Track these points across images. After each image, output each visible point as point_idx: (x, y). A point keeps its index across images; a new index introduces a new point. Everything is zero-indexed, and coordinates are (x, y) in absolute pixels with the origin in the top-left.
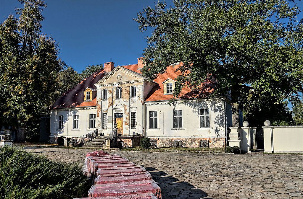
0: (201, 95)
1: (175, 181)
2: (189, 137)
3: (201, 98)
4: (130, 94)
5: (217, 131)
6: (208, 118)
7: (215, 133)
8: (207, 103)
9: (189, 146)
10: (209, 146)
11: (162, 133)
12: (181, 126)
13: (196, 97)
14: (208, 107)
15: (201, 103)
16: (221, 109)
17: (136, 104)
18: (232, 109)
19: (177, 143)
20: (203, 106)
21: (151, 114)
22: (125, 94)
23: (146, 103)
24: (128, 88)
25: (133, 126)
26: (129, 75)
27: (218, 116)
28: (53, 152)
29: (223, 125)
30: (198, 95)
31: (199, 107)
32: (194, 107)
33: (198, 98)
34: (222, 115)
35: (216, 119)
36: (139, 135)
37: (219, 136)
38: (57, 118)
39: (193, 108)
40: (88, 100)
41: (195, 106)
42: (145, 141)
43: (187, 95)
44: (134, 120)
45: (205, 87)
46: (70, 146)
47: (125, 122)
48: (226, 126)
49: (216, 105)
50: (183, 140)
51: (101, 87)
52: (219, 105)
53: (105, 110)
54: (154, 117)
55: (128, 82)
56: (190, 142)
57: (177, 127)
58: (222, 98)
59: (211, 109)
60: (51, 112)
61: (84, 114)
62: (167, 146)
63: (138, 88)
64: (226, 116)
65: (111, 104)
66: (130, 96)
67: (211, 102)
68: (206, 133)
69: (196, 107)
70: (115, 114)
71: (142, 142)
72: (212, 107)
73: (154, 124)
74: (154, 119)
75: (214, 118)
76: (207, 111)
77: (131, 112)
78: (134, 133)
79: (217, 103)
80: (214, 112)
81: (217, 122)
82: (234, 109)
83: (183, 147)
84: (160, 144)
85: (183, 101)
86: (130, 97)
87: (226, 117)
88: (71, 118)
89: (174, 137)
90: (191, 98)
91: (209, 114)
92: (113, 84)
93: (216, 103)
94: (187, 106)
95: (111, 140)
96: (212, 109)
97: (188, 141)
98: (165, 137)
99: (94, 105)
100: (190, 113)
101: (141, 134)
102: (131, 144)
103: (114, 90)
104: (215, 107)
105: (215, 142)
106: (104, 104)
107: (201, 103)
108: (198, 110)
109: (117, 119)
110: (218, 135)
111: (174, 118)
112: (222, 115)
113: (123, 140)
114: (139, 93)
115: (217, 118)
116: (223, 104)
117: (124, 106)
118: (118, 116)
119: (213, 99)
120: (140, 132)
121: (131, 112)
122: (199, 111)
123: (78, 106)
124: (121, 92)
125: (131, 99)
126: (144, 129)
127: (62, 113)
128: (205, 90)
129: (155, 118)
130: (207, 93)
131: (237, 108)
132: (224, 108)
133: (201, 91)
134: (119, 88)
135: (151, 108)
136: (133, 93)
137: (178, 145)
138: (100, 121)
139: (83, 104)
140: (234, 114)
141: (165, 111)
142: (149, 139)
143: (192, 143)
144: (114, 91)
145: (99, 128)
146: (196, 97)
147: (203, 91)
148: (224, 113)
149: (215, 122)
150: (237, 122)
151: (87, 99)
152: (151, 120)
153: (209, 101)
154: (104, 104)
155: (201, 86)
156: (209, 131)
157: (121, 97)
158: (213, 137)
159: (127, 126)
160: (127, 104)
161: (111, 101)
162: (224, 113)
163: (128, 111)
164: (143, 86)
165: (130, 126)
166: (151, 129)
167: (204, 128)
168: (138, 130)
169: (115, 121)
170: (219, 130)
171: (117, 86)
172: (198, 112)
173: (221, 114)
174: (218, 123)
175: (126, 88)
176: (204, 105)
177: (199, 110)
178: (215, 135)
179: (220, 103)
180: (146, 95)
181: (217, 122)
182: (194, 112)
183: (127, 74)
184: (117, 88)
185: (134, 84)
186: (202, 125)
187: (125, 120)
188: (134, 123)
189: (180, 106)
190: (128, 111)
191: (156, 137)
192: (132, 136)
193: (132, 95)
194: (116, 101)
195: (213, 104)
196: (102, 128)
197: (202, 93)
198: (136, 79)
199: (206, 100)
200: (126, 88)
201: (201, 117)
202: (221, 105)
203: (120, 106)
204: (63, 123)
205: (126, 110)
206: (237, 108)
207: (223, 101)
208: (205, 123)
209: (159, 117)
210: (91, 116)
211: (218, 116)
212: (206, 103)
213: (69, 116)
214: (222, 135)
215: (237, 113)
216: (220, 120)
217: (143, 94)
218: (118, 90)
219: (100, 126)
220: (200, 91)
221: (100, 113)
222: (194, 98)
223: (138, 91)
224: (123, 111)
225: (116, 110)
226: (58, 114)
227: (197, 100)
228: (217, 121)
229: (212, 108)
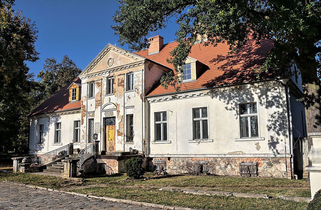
0: (239, 78)
2: (220, 156)
3: (240, 83)
4: (125, 85)
5: (273, 144)
6: (255, 120)
7: (270, 147)
8: (253, 92)
9: (220, 173)
10: (257, 174)
11: (176, 148)
12: (206, 136)
13: (231, 81)
14: (253, 98)
15: (241, 93)
16: (280, 100)
18: (305, 97)
19: (200, 167)
20: (245, 98)
21: (157, 115)
22: (119, 86)
23: (148, 99)
24: (122, 77)
25: (130, 138)
27: (274, 115)
29: (285, 132)
30: (235, 79)
31: (237, 100)
32: (229, 101)
33: (235, 84)
34: (283, 112)
35: (269, 121)
36: (137, 152)
37: (279, 154)
38: (37, 128)
39: (226, 102)
40: (74, 100)
41: (230, 99)
42: (131, 165)
43: (216, 80)
44: (132, 128)
45: (246, 67)
46: (21, 171)
48: (291, 133)
49: (269, 93)
50: (210, 160)
52: (275, 94)
54: (162, 122)
55: (122, 68)
56: (223, 165)
57: (199, 137)
58: (281, 80)
59: (261, 103)
60: (31, 120)
61: (67, 121)
62: (183, 172)
63: (136, 75)
64: (290, 114)
65: (99, 103)
66: (125, 89)
67: (260, 89)
68: (249, 149)
69: (232, 101)
70: (105, 119)
71: (138, 166)
72: (262, 98)
73: (161, 133)
74: (162, 125)
75: (267, 119)
76: (253, 105)
77: (127, 115)
78: (131, 148)
79: (272, 90)
80: (267, 107)
81: (273, 127)
82: (309, 97)
83: (209, 174)
84: (171, 167)
85: (208, 91)
86: (125, 90)
87: (291, 117)
88: (52, 127)
89: (194, 156)
90: (222, 85)
93: (270, 90)
94: (216, 100)
95: (70, 163)
96: (263, 103)
98: (157, 156)
99: (76, 107)
100: (221, 112)
101: (140, 149)
102: (117, 168)
103: (103, 82)
104: (267, 99)
105: (270, 165)
107: (241, 93)
108: (236, 105)
109: (107, 127)
110: (275, 151)
112: (281, 114)
113: (105, 161)
114: (138, 83)
115: (271, 119)
116: (284, 91)
117: (117, 105)
119: (263, 83)
121: (127, 115)
122: (237, 108)
123: (60, 110)
124: (113, 83)
126: (146, 142)
128: (249, 69)
129: (203, 121)
130: (252, 73)
131: (316, 94)
132: (285, 99)
133: (240, 72)
134: (110, 78)
135: (156, 107)
137: (201, 169)
138: (85, 130)
139: (66, 108)
140: (309, 106)
142: (151, 159)
143: (226, 167)
144: (104, 82)
145: (84, 141)
146: (231, 81)
147: (244, 71)
148: (285, 108)
149: (268, 126)
150: (316, 123)
151: (73, 99)
152: (158, 127)
153: (255, 87)
155: (242, 65)
159: (121, 138)
160: (120, 102)
161: (99, 99)
162: (285, 108)
163: (121, 114)
164: (144, 72)
165: (125, 137)
167: (159, 142)
168: (137, 145)
169: (106, 129)
170: (278, 143)
171: (107, 75)
172: (236, 109)
173: (281, 110)
174: (275, 128)
175: (119, 77)
176: (247, 95)
177: (238, 106)
178: (269, 152)
179: (278, 90)
180: (151, 86)
181: (273, 127)
183: (121, 55)
184: (107, 78)
185: (130, 70)
186: (244, 133)
187: (117, 128)
188: (132, 133)
189: (203, 100)
190: (121, 114)
191: (165, 156)
192: (120, 155)
193: (128, 88)
195: (264, 93)
197: (242, 75)
198: (133, 61)
199: (249, 86)
200: (119, 76)
201: (241, 118)
202: (280, 93)
203: (112, 106)
204: (44, 134)
205: (118, 112)
206: (316, 94)
207: (283, 85)
208: (248, 129)
211: (274, 115)
212: (251, 92)
213: (50, 125)
214: (283, 152)
215: (317, 104)
216: (278, 123)
217: (144, 84)
218: (109, 82)
219: (85, 137)
220: (239, 73)
221: (85, 118)
222: (227, 85)
224: (115, 114)
225: (106, 111)
226: (38, 123)
227: (234, 87)
228: (274, 124)
229: (261, 100)
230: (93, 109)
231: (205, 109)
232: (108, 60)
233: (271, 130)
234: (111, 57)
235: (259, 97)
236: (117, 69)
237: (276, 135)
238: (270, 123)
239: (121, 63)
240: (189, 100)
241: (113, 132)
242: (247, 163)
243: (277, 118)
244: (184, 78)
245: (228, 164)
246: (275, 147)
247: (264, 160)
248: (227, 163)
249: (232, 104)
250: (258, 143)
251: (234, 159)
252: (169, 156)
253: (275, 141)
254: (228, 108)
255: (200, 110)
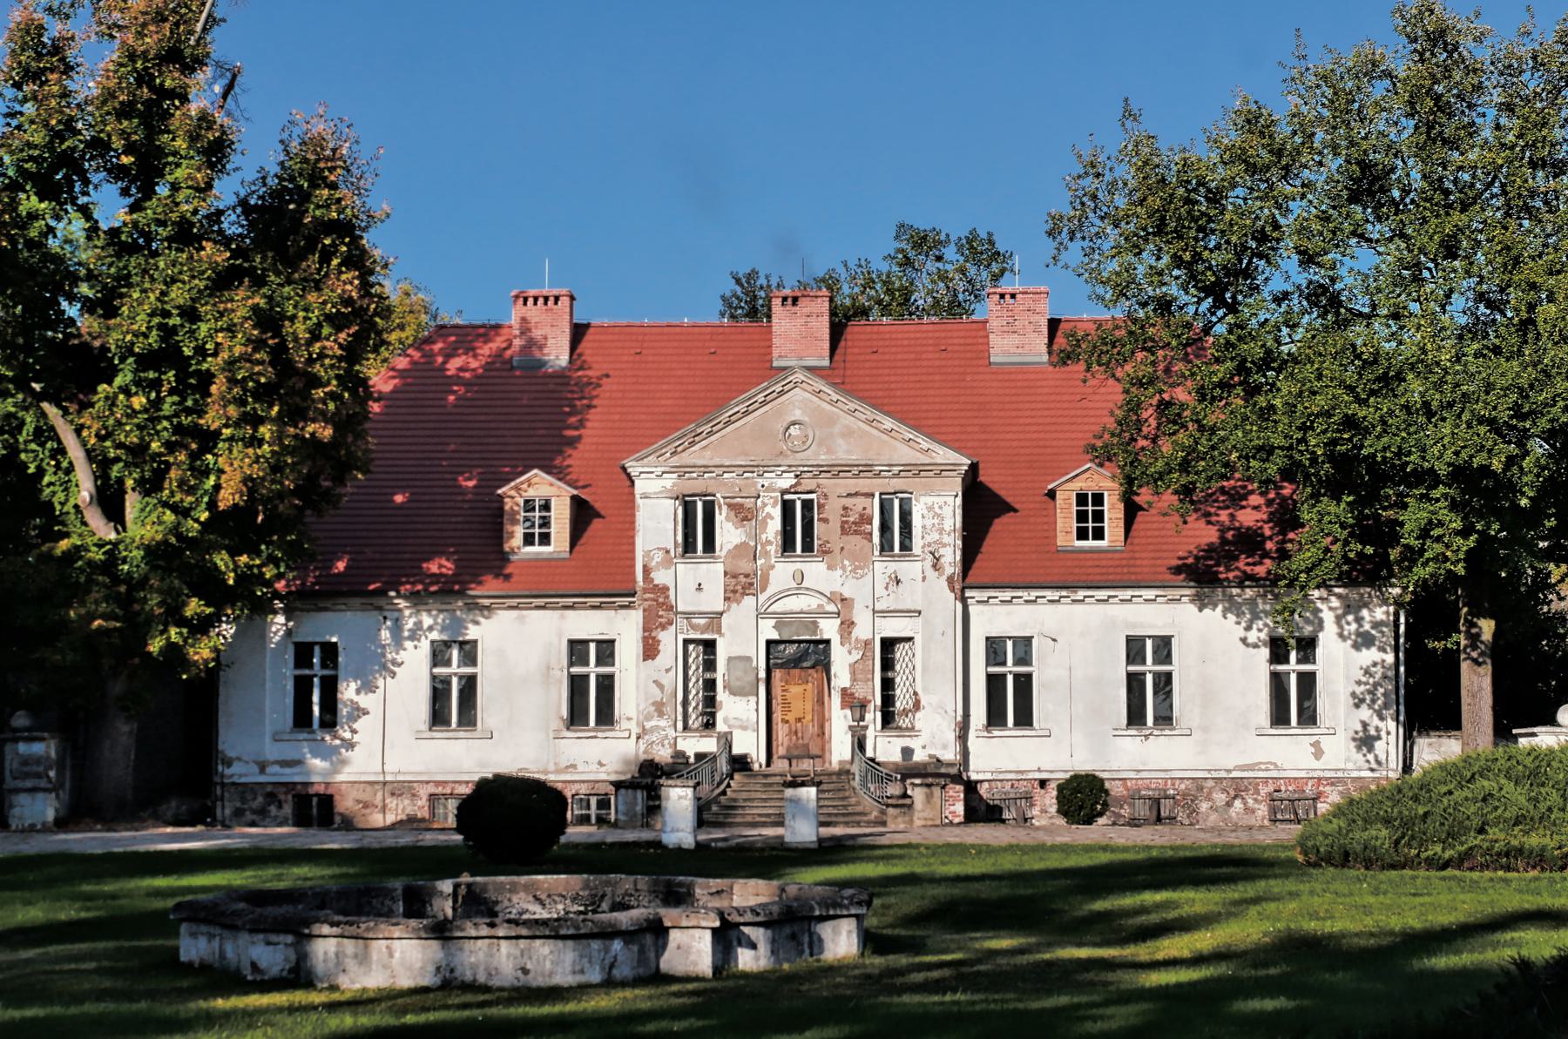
1: (226, 993)
2: (1215, 775)
6: (1308, 683)
17: (909, 598)
21: (994, 648)
23: (968, 593)
24: (860, 503)
26: (867, 428)
28: (777, 716)
35: (1359, 683)
41: (1256, 616)
47: (844, 690)
49: (1365, 613)
50: (1183, 786)
51: (669, 481)
53: (702, 621)
54: (592, 670)
55: (866, 470)
56: (1220, 798)
61: (519, 645)
65: (741, 585)
68: (1291, 755)
69: (1260, 623)
70: (769, 643)
73: (1010, 700)
74: (1010, 679)
81: (1368, 697)
85: (1192, 591)
89: (1132, 775)
91: (1170, 663)
92: (762, 468)
97: (1210, 793)
98: (1001, 777)
100: (1218, 647)
104: (1361, 626)
106: (697, 585)
109: (777, 674)
111: (434, 677)
114: (936, 536)
115: (1364, 679)
118: (798, 656)
120: (945, 747)
125: (883, 568)
127: (332, 627)
136: (896, 532)
141: (1077, 638)
143: (1229, 804)
144: (768, 509)
149: (1353, 695)
152: (995, 684)
154: (697, 585)
156: (1316, 745)
157: (808, 547)
158: (1340, 774)
163: (862, 631)
166: (996, 733)
168: (931, 737)
170: (1379, 738)
171: (787, 481)
174: (1374, 701)
175: (849, 502)
181: (1368, 697)
182: (1248, 645)
183: (848, 420)
184: (784, 492)
189: (1153, 613)
191: (1030, 776)
193: (886, 547)
194: (782, 572)
196: (680, 725)
198: (905, 454)
205: (847, 626)
208: (1293, 703)
209: (1043, 673)
210: (577, 650)
213: (408, 644)
216: (1381, 690)
218: (787, 508)
223: (929, 523)
224: (829, 629)
225: (781, 622)
226: (289, 633)
228: (1369, 692)
229: (1341, 627)
230: (713, 599)
231: (1024, 645)
232: (785, 425)
233: (1364, 706)
234: (797, 414)
235: (1338, 619)
236: (837, 470)
237: (1375, 718)
238: (1363, 688)
239: (848, 452)
240: (1116, 611)
241: (809, 695)
242: (1287, 791)
243: (1378, 676)
244: (529, 539)
245: (1235, 797)
246: (1371, 749)
247: (1332, 784)
248: (1232, 793)
249: (1260, 630)
250: (1318, 742)
251: (1255, 783)
252: (1044, 776)
253: (1373, 732)
254: (1250, 640)
255: (592, 646)
